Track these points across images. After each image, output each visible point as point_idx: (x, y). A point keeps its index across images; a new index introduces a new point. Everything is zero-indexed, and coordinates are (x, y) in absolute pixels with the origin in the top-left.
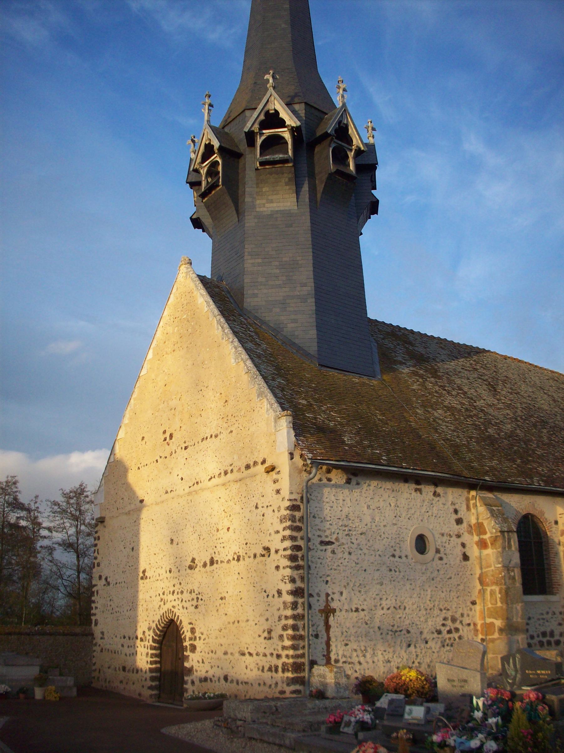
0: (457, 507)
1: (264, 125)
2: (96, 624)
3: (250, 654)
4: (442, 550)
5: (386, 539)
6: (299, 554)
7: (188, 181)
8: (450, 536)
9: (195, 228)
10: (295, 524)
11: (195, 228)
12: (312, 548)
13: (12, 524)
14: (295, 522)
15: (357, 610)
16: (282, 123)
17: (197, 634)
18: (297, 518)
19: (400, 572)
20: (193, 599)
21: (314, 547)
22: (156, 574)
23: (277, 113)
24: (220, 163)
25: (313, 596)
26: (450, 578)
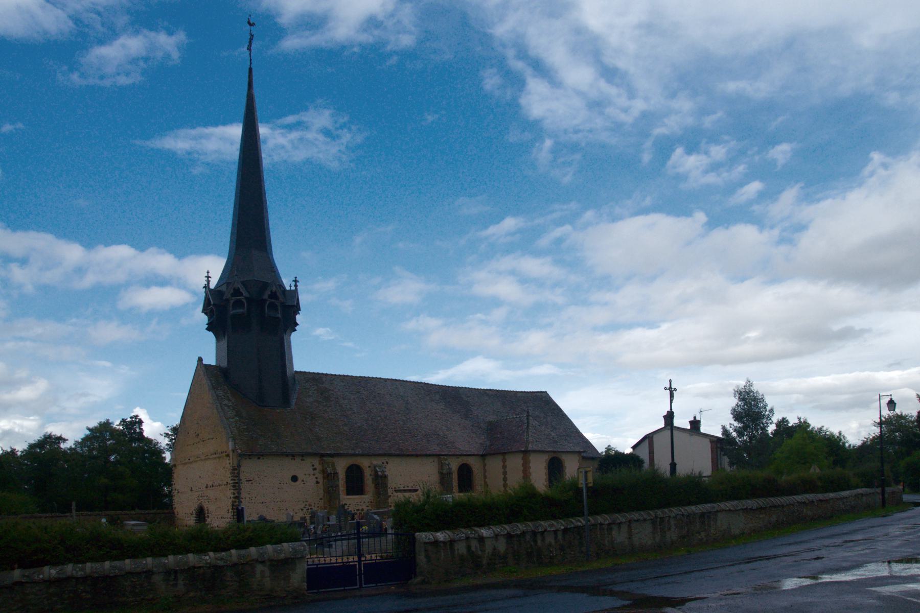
1: (233, 295)
2: (175, 509)
8: (310, 475)
13: (47, 565)
16: (241, 294)
23: (239, 289)
24: (215, 310)
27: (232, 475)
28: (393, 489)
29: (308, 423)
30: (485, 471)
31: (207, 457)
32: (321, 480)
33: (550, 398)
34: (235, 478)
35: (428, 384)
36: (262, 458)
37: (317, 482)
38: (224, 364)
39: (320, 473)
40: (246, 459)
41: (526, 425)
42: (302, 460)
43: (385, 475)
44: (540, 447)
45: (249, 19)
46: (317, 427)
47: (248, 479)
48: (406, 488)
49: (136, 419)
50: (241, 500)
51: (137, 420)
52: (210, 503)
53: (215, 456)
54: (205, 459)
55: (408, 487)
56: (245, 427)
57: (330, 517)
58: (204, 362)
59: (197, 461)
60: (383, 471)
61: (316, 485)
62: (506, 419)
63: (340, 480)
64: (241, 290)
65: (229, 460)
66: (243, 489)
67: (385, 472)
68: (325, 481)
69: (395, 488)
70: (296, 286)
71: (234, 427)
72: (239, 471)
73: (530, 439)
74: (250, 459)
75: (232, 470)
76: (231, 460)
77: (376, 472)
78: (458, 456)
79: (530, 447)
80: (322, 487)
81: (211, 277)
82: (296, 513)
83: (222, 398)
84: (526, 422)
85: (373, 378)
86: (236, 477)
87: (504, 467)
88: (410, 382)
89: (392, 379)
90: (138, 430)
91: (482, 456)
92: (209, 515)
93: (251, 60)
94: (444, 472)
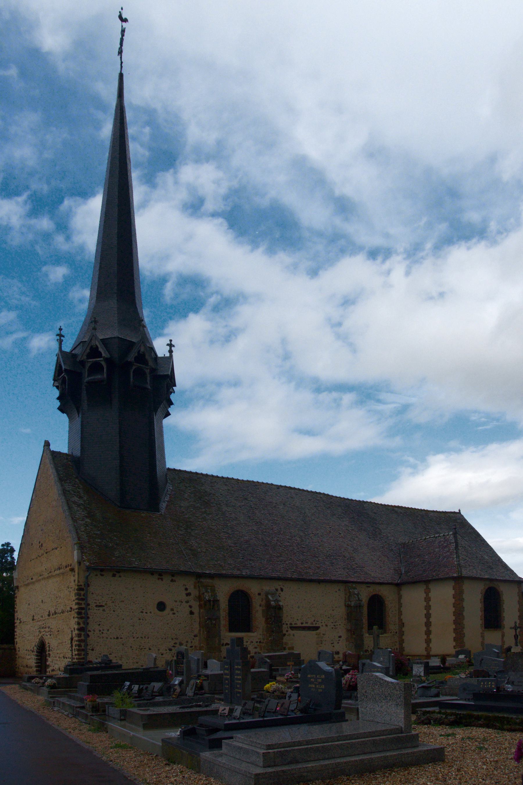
0: (187, 587)
1: (89, 356)
2: (17, 644)
3: (66, 658)
4: (175, 609)
5: (137, 604)
6: (83, 611)
7: (54, 385)
8: (182, 602)
10: (80, 597)
12: (91, 608)
14: (81, 596)
15: (117, 638)
16: (100, 355)
17: (51, 648)
18: (82, 594)
19: (146, 620)
20: (49, 631)
21: (92, 608)
22: (37, 618)
23: (97, 347)
25: (91, 631)
26: (180, 623)
27: (77, 597)
28: (289, 625)
29: (180, 532)
30: (400, 605)
31: (50, 574)
32: (196, 610)
33: (465, 520)
34: (80, 602)
35: (328, 495)
36: (118, 575)
37: (192, 613)
38: (77, 453)
39: (194, 600)
40: (97, 575)
41: (454, 544)
42: (172, 581)
43: (280, 605)
44: (474, 573)
45: (120, 12)
47: (98, 604)
48: (304, 625)
49: (8, 546)
50: (89, 633)
51: (9, 548)
52: (52, 636)
53: (58, 572)
54: (48, 578)
55: (306, 623)
56: (99, 532)
57: (209, 662)
58: (53, 448)
59: (40, 580)
60: (276, 600)
61: (190, 616)
62: (425, 539)
63: (221, 611)
64: (100, 349)
65: (74, 576)
66: (91, 617)
67: (280, 601)
68: (202, 611)
69: (291, 624)
70: (171, 351)
71: (83, 531)
72: (87, 591)
73: (462, 562)
74: (102, 575)
75: (78, 590)
76: (77, 576)
77: (268, 601)
78: (368, 585)
79: (465, 573)
80: (198, 620)
81: (63, 336)
82: (162, 654)
84: (453, 541)
85: (263, 483)
86: (82, 599)
87: (428, 599)
88: (307, 491)
89: (285, 487)
90: (9, 558)
91: (398, 585)
92: (50, 652)
93: (122, 63)
94: (353, 604)
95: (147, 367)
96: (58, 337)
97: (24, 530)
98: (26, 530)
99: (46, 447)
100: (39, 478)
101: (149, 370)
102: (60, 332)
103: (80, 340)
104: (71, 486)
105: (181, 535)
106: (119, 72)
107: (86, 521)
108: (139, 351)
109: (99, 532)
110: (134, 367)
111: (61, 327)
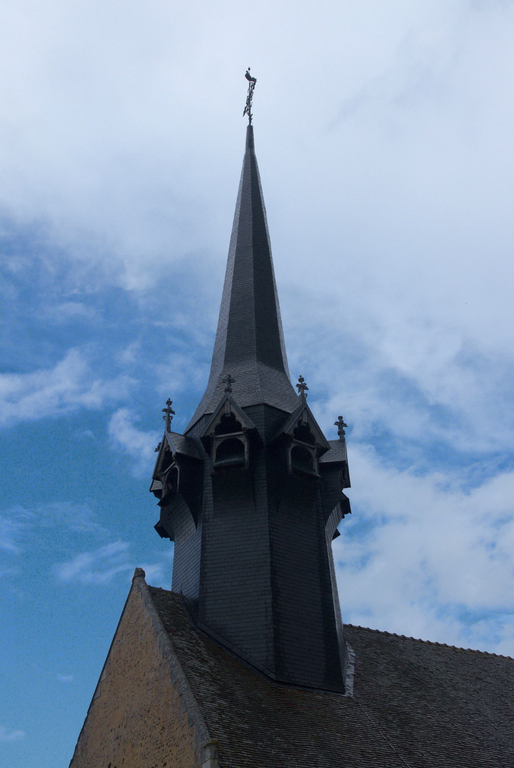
1: (220, 429)
7: (152, 489)
9: (162, 538)
11: (162, 538)
16: (238, 427)
23: (233, 415)
24: (178, 470)
45: (247, 72)
46: (420, 745)
56: (246, 726)
58: (149, 579)
64: (238, 418)
71: (217, 723)
83: (186, 654)
95: (312, 446)
96: (165, 414)
97: (77, 747)
98: (79, 747)
99: (137, 581)
100: (118, 638)
101: (315, 451)
102: (169, 406)
103: (201, 414)
104: (185, 641)
105: (396, 737)
106: (248, 124)
107: (219, 704)
108: (300, 422)
109: (246, 726)
110: (293, 445)
111: (169, 399)
